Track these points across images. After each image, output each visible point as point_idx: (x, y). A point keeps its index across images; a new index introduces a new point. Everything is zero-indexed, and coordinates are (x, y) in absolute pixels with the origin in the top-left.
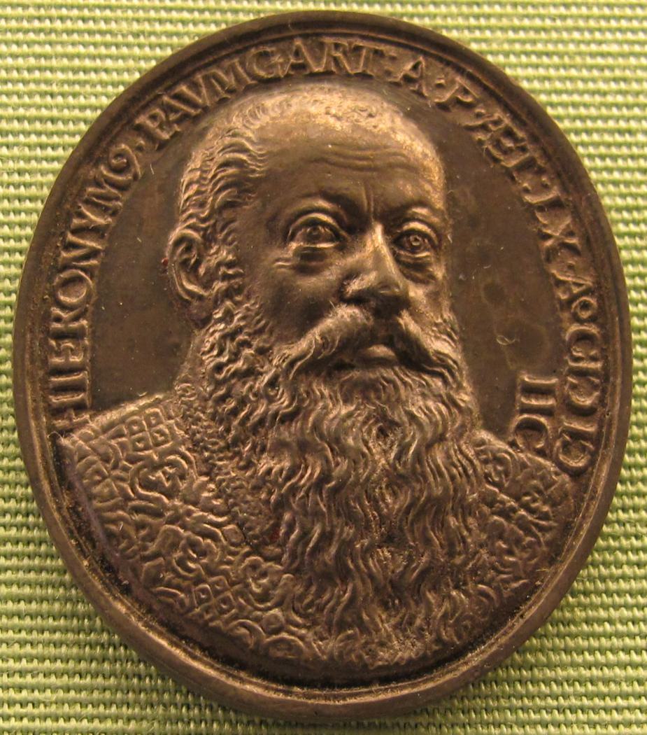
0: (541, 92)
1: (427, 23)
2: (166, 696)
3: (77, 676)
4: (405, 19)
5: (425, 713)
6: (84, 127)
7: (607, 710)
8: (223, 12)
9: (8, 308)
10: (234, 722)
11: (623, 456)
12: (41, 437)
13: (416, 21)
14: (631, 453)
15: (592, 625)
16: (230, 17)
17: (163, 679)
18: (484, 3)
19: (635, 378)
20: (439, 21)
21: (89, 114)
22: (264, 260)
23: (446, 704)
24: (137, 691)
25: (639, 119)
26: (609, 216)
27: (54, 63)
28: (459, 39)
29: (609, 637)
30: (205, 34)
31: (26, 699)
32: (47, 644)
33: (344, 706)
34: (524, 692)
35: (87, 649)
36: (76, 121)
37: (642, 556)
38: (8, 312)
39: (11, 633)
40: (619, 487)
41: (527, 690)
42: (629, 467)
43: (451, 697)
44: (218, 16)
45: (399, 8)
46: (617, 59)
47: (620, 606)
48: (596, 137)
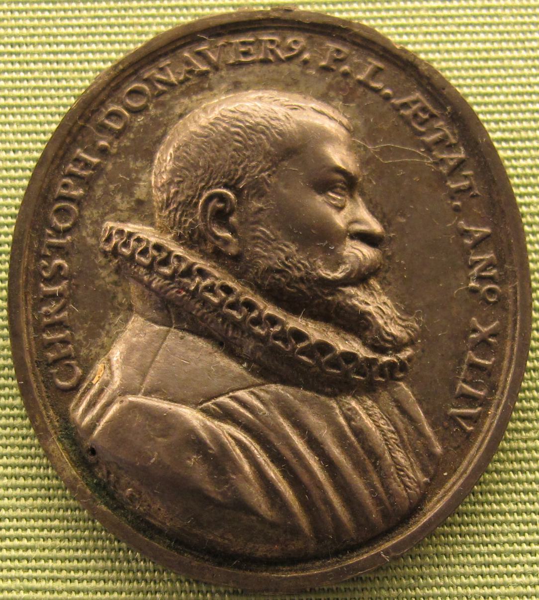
1: (344, 16)
2: (147, 574)
3: (49, 520)
4: (329, 14)
6: (58, 119)
9: (7, 246)
10: (196, 591)
12: (30, 344)
13: (337, 15)
15: (488, 515)
16: (174, 20)
17: (145, 561)
20: (360, 14)
21: (113, 56)
22: (149, 194)
24: (145, 592)
26: (507, 171)
27: (509, 80)
29: (500, 524)
33: (277, 577)
34: (442, 583)
35: (127, 584)
38: (6, 352)
48: (515, 107)
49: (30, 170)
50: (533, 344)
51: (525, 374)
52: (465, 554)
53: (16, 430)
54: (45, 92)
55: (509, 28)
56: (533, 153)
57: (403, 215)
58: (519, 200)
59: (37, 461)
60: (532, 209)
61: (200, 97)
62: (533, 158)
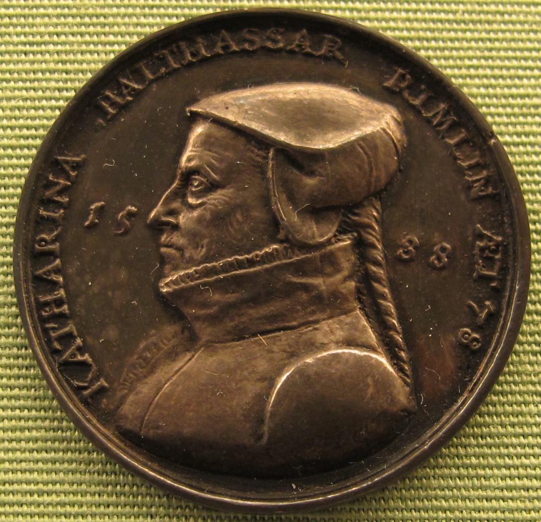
0: (446, 68)
4: (323, 12)
5: (365, 501)
7: (509, 456)
8: (182, 7)
11: (525, 205)
14: (530, 313)
16: (187, 11)
18: (444, 2)
19: (531, 288)
21: (62, 103)
23: (380, 495)
25: (534, 59)
28: (371, 28)
30: (169, 24)
31: (51, 512)
32: (67, 472)
36: (52, 109)
37: (536, 503)
39: (6, 421)
40: (517, 347)
41: (446, 462)
42: (528, 323)
43: (383, 490)
44: (179, 11)
45: (318, 4)
46: (514, 80)
47: (529, 435)
49: (36, 148)
50: (535, 267)
51: (531, 277)
52: (526, 436)
53: (31, 444)
54: (35, 48)
55: (526, 54)
56: (534, 54)
57: (494, 288)
58: (528, 206)
59: (46, 403)
60: (534, 187)
61: (299, 106)
62: (533, 384)
